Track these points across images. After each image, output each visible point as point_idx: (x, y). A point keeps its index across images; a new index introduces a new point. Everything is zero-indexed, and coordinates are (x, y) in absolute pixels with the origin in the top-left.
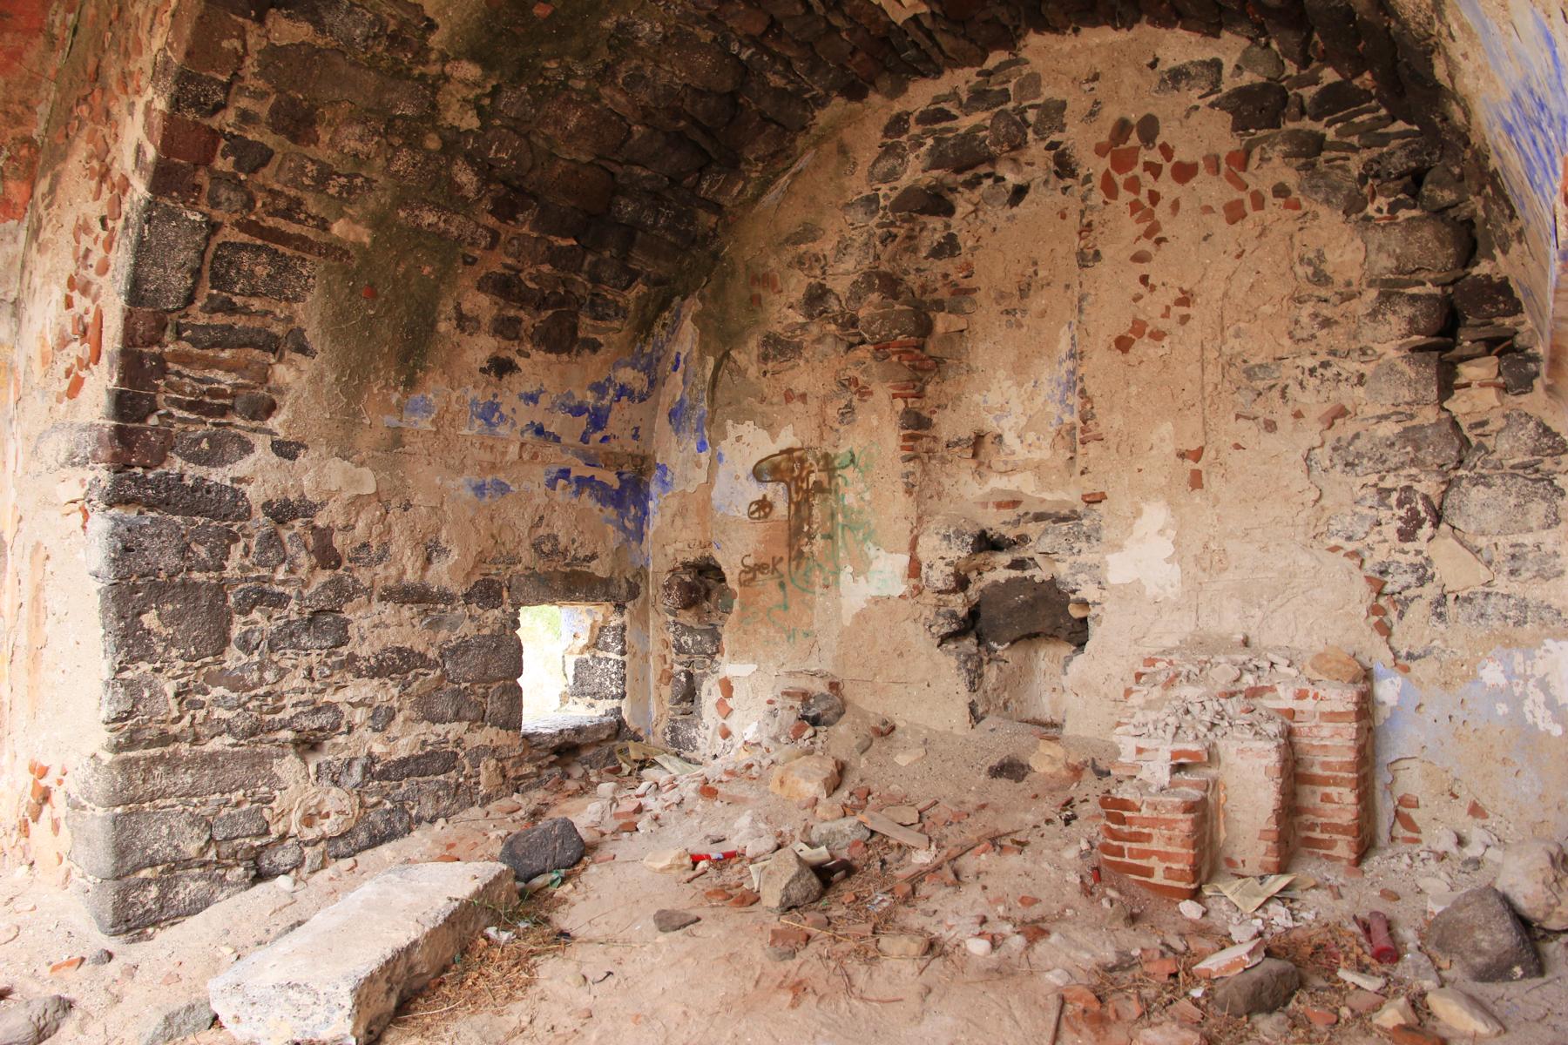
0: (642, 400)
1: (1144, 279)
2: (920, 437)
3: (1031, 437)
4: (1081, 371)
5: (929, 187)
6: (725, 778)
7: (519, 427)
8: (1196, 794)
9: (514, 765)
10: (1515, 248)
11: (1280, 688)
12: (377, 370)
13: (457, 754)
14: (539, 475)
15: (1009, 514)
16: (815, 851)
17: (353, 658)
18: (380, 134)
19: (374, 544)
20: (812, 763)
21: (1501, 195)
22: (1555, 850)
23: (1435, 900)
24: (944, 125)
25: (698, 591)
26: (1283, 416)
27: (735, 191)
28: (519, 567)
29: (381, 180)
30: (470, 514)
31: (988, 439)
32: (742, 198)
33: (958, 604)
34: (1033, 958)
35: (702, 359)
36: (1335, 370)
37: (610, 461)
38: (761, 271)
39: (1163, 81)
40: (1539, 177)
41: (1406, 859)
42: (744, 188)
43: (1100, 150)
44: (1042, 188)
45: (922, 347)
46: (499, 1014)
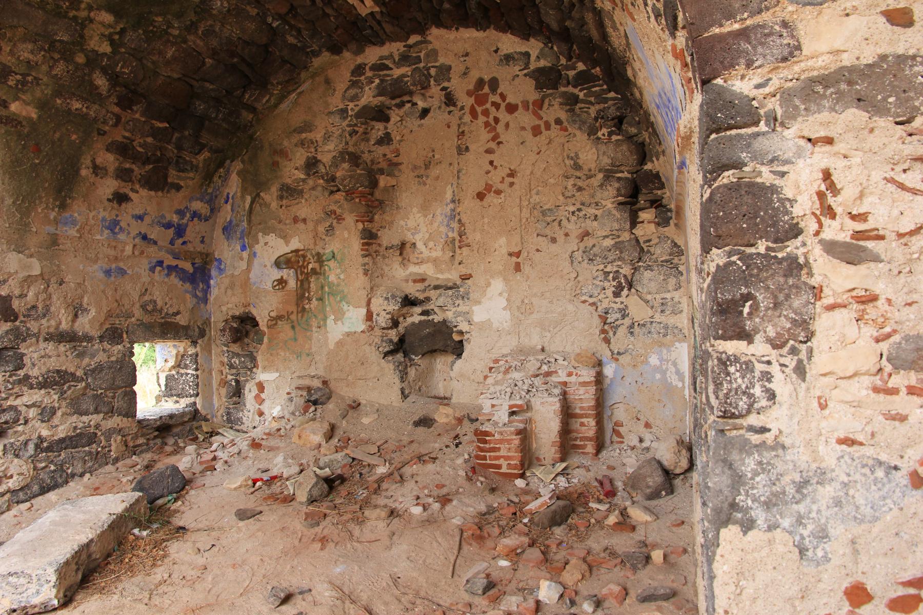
0: (206, 220)
1: (491, 163)
2: (371, 244)
3: (431, 244)
4: (458, 210)
5: (376, 106)
6: (265, 437)
7: (132, 235)
8: (521, 426)
9: (132, 438)
10: (661, 157)
11: (560, 371)
12: (40, 198)
13: (96, 434)
14: (145, 264)
15: (420, 286)
16: (323, 471)
17: (27, 377)
18: (45, 50)
19: (40, 306)
20: (317, 425)
21: (655, 133)
22: (678, 438)
23: (630, 467)
24: (385, 72)
25: (241, 332)
26: (561, 239)
27: (264, 100)
28: (133, 319)
29: (45, 79)
30: (102, 287)
31: (408, 246)
32: (268, 105)
33: (393, 335)
34: (445, 513)
35: (243, 197)
36: (584, 213)
37: (189, 256)
39: (501, 60)
40: (669, 130)
41: (618, 451)
42: (270, 99)
43: (469, 93)
45: (372, 194)
46: (149, 575)
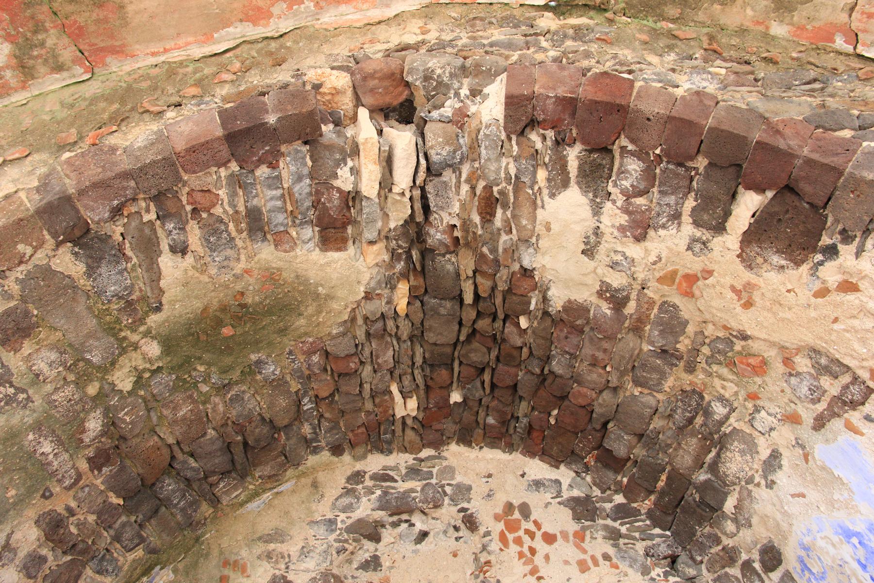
24: (388, 484)
27: (234, 495)
32: (235, 501)
38: (233, 558)
39: (529, 485)
43: (497, 518)
44: (441, 535)
